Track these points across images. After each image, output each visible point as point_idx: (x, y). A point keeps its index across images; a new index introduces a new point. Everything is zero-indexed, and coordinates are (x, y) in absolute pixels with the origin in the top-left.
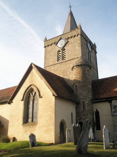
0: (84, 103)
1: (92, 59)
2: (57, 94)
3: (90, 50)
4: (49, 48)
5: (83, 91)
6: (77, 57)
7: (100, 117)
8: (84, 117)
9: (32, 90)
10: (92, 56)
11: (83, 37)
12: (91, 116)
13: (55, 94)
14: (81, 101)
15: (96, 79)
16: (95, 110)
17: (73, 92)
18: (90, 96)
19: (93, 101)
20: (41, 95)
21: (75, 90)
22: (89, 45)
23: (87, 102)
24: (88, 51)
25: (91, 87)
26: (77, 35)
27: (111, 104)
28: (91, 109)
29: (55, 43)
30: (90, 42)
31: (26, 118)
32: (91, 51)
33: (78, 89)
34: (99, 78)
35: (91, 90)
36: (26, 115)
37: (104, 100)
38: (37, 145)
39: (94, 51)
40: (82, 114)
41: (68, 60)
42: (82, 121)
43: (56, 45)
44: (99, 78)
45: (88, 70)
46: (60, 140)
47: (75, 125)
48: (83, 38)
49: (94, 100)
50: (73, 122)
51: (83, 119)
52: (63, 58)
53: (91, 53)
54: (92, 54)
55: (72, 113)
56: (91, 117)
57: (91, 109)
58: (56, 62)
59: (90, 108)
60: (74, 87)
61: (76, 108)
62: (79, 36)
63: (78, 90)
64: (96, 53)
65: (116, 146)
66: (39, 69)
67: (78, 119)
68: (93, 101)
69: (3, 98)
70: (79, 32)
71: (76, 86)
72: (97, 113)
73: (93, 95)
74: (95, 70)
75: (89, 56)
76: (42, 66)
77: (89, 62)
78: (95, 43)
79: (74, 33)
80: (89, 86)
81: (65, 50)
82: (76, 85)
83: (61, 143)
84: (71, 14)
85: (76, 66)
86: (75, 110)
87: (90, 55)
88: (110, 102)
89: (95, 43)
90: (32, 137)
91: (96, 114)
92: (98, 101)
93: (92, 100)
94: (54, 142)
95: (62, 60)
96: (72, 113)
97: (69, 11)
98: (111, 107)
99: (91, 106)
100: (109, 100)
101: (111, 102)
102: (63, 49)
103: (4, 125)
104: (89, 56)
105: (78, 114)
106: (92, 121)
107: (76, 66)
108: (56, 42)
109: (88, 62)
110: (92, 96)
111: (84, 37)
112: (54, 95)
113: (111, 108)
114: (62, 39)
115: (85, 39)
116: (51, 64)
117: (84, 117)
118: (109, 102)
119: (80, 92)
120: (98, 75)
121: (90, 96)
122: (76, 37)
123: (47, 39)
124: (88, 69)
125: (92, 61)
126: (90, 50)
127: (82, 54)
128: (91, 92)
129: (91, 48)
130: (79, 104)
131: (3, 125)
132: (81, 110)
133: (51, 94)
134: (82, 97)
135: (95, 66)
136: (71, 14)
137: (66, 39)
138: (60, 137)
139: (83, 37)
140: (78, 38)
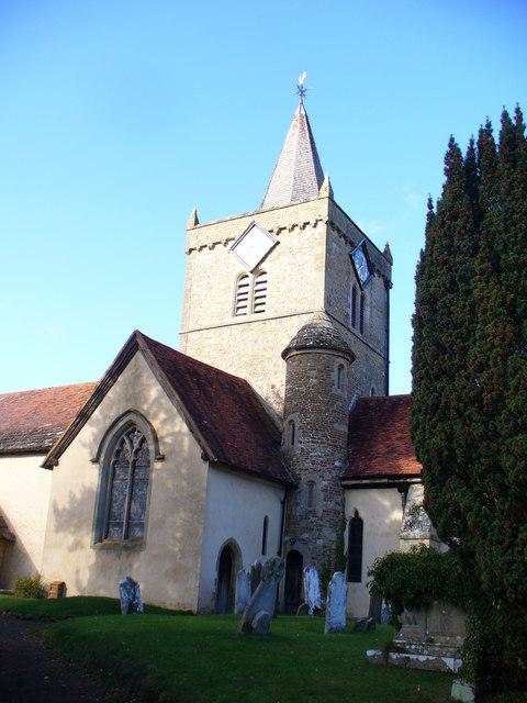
0: (312, 484)
1: (367, 313)
2: (217, 456)
3: (364, 276)
5: (313, 442)
8: (306, 536)
9: (130, 428)
10: (368, 299)
11: (339, 230)
12: (334, 535)
13: (211, 454)
14: (304, 479)
15: (379, 394)
16: (350, 514)
17: (278, 444)
18: (337, 464)
19: (345, 483)
21: (287, 437)
22: (359, 257)
25: (345, 429)
26: (313, 222)
28: (339, 508)
30: (367, 246)
31: (105, 523)
32: (369, 280)
33: (299, 433)
34: (392, 393)
35: (342, 443)
36: (106, 514)
37: (386, 480)
38: (141, 610)
39: (381, 280)
40: (303, 524)
42: (299, 547)
45: (341, 365)
46: (217, 604)
48: (335, 234)
49: (348, 479)
50: (268, 550)
51: (303, 540)
52: (258, 306)
53: (366, 291)
54: (372, 294)
55: (266, 520)
56: (334, 537)
57: (339, 508)
58: (229, 319)
59: (331, 505)
60: (286, 423)
61: (283, 503)
62: (322, 227)
63: (296, 441)
64: (388, 285)
66: (154, 346)
67: (287, 538)
68: (345, 483)
69: (13, 436)
70: (323, 211)
71: (292, 421)
72: (357, 524)
73: (350, 459)
74: (376, 356)
77: (353, 326)
78: (387, 246)
82: (290, 418)
83: (216, 611)
85: (297, 349)
87: (363, 297)
89: (387, 246)
90: (131, 585)
91: (352, 525)
94: (195, 609)
96: (266, 520)
99: (339, 499)
101: (406, 492)
105: (288, 522)
106: (336, 550)
107: (297, 349)
109: (351, 327)
110: (345, 462)
111: (341, 228)
115: (345, 237)
116: (206, 324)
117: (306, 536)
118: (400, 491)
119: (301, 446)
121: (337, 464)
124: (342, 361)
125: (367, 320)
126: (364, 276)
127: (328, 302)
128: (341, 448)
129: (369, 269)
132: (298, 512)
134: (308, 464)
135: (381, 336)
138: (218, 595)
139: (339, 230)
140: (316, 236)
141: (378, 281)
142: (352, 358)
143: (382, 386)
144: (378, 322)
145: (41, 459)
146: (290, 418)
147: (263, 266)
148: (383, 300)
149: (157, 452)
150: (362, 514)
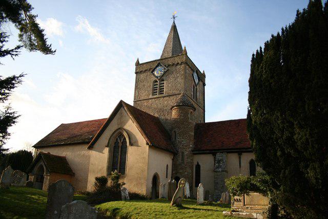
0: (183, 153)
1: (198, 94)
4: (142, 76)
6: (178, 92)
7: (201, 172)
8: (181, 171)
9: (121, 135)
11: (189, 65)
15: (202, 122)
20: (132, 142)
21: (173, 137)
22: (195, 75)
23: (186, 153)
24: (194, 83)
25: (193, 134)
27: (215, 158)
29: (150, 69)
30: (198, 71)
32: (198, 83)
34: (206, 122)
35: (192, 138)
41: (167, 95)
43: (152, 72)
44: (206, 121)
47: (170, 182)
54: (199, 88)
58: (151, 96)
59: (189, 160)
61: (173, 160)
64: (204, 85)
65: (283, 216)
72: (198, 167)
75: (195, 89)
76: (132, 104)
79: (177, 60)
80: (190, 133)
81: (163, 80)
84: (174, 28)
85: (176, 106)
86: (171, 162)
88: (214, 154)
92: (201, 152)
93: (193, 151)
95: (159, 94)
97: (171, 23)
98: (215, 160)
100: (213, 152)
102: (162, 79)
103: (76, 173)
104: (195, 89)
107: (176, 106)
108: (151, 69)
112: (147, 144)
113: (215, 162)
114: (161, 65)
117: (181, 171)
120: (204, 115)
122: (178, 67)
123: (140, 62)
124: (192, 111)
126: (197, 81)
130: (177, 154)
131: (74, 174)
133: (145, 142)
134: (181, 146)
135: (202, 103)
136: (174, 28)
137: (165, 66)
141: (201, 83)
142: (195, 109)
143: (203, 120)
144: (201, 98)
145: (86, 146)
146: (174, 130)
147: (164, 78)
148: (203, 90)
149: (130, 143)
150: (200, 163)
